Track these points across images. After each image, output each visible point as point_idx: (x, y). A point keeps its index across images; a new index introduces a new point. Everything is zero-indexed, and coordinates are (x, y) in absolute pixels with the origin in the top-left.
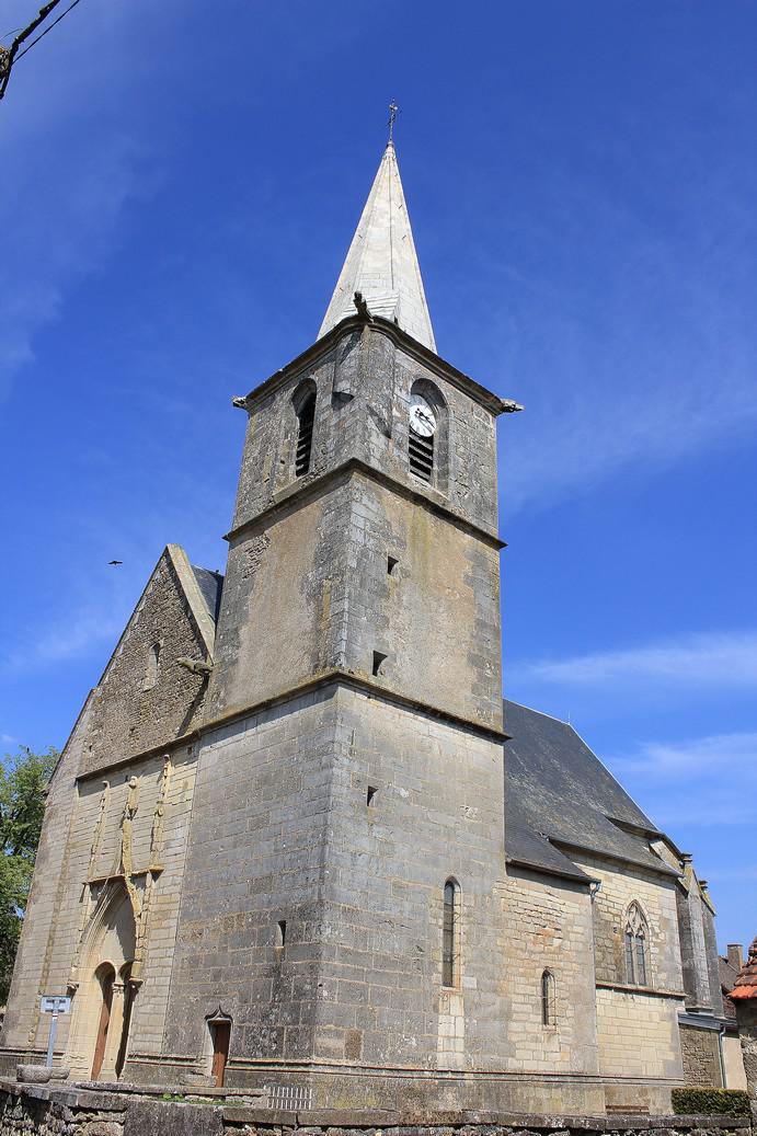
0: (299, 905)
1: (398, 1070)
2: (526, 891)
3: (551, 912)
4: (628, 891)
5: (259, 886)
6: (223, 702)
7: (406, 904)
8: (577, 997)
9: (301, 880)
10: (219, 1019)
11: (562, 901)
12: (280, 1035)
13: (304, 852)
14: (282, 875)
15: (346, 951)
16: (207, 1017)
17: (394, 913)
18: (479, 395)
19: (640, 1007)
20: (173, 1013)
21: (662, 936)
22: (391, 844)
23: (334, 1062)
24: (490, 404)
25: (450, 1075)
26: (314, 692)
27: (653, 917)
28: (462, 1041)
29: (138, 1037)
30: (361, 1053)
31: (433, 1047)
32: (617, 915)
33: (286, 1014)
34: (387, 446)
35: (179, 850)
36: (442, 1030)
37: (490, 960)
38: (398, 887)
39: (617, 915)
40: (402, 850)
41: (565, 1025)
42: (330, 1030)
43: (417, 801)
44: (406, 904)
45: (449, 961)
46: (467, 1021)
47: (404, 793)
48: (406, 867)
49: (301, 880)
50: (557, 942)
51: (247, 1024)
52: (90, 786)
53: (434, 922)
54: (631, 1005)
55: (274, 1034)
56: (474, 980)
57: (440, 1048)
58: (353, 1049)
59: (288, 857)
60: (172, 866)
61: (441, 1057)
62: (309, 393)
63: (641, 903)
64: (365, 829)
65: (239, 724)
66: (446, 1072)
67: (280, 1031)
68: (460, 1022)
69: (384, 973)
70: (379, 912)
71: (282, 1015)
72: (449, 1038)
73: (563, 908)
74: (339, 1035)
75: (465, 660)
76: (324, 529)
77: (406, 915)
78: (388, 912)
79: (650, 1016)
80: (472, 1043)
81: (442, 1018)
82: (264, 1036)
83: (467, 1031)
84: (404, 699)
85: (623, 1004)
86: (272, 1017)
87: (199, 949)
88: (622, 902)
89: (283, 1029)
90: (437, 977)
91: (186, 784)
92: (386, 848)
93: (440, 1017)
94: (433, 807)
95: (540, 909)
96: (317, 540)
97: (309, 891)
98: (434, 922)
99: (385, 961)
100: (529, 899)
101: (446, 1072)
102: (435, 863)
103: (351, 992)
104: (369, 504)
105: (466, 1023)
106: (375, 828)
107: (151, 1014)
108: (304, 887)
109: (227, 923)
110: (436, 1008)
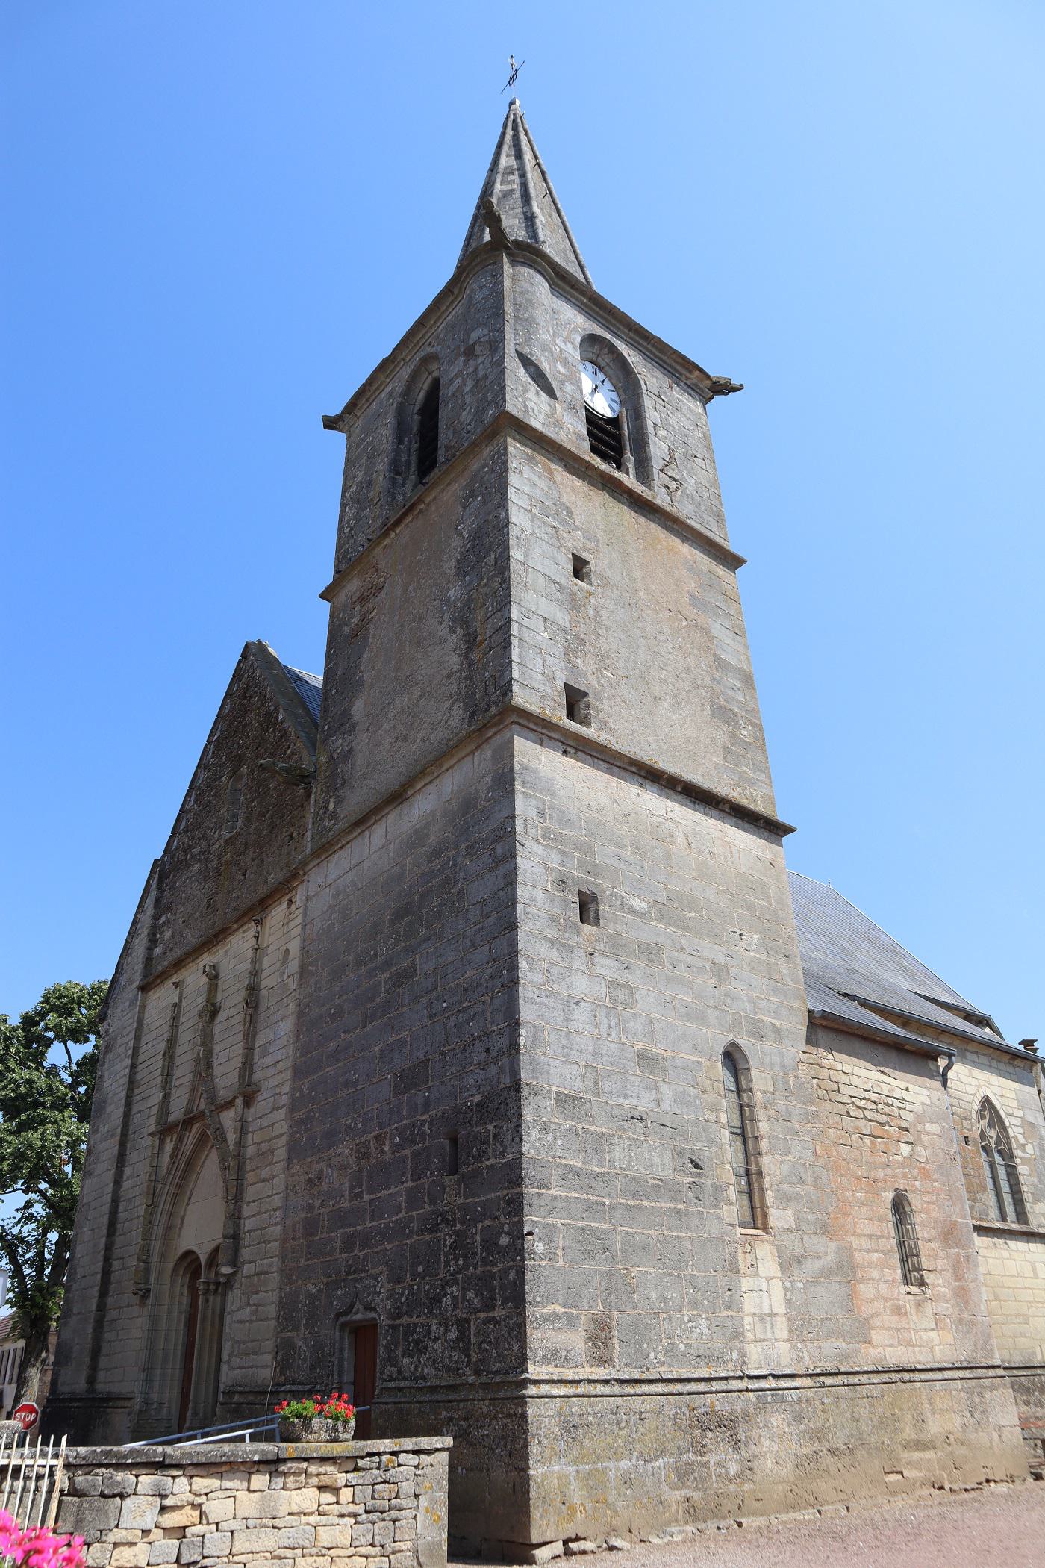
0: (477, 1098)
1: (689, 1380)
2: (848, 1069)
3: (890, 1101)
4: (974, 1082)
5: (410, 1079)
6: (334, 816)
7: (664, 1088)
8: (949, 1235)
9: (477, 1055)
10: (359, 1317)
11: (903, 1085)
12: (463, 1333)
13: (478, 1008)
14: (444, 1054)
15: (570, 1169)
16: (338, 1315)
17: (645, 1103)
18: (679, 368)
19: (1015, 1256)
20: (287, 1317)
21: (1029, 1148)
22: (628, 986)
23: (570, 1374)
24: (695, 381)
25: (772, 1383)
26: (473, 752)
27: (1013, 1121)
28: (784, 1319)
29: (236, 1361)
30: (615, 1355)
31: (738, 1335)
32: (965, 1118)
33: (471, 1294)
34: (553, 408)
35: (280, 1055)
36: (749, 1304)
37: (810, 1180)
38: (646, 1059)
39: (965, 1118)
40: (647, 1000)
41: (939, 1282)
42: (555, 1316)
43: (660, 919)
44: (664, 1088)
45: (752, 1180)
46: (787, 1284)
47: (638, 904)
48: (656, 1025)
49: (477, 1055)
50: (905, 1149)
51: (405, 1320)
52: (158, 994)
53: (712, 1117)
54: (1005, 1254)
55: (453, 1334)
56: (790, 1212)
57: (749, 1335)
58: (600, 1337)
59: (453, 1021)
60: (271, 1083)
61: (754, 1351)
62: (430, 379)
63: (994, 1100)
64: (579, 961)
65: (359, 839)
66: (764, 1377)
67: (463, 1325)
68: (777, 1287)
69: (640, 1207)
70: (620, 1101)
71: (464, 1296)
72: (762, 1318)
73: (906, 1095)
74: (572, 1322)
75: (707, 712)
76: (466, 528)
77: (665, 1105)
78: (635, 1101)
79: (1034, 1269)
80: (800, 1327)
81: (746, 1283)
82: (436, 1339)
83: (789, 1302)
84: (621, 756)
85: (994, 1253)
86: (447, 1301)
87: (318, 1203)
88: (969, 1098)
89: (468, 1321)
90: (732, 1209)
91: (287, 951)
92: (622, 995)
93: (743, 1280)
94: (687, 929)
95: (874, 1097)
96: (456, 542)
97: (494, 1070)
98: (712, 1117)
99: (638, 1187)
100: (855, 1081)
101: (764, 1377)
102: (701, 1019)
103: (592, 1245)
104: (534, 478)
105: (786, 1290)
106: (597, 958)
107: (251, 1321)
108: (483, 1066)
109: (362, 1154)
110: (733, 1265)
